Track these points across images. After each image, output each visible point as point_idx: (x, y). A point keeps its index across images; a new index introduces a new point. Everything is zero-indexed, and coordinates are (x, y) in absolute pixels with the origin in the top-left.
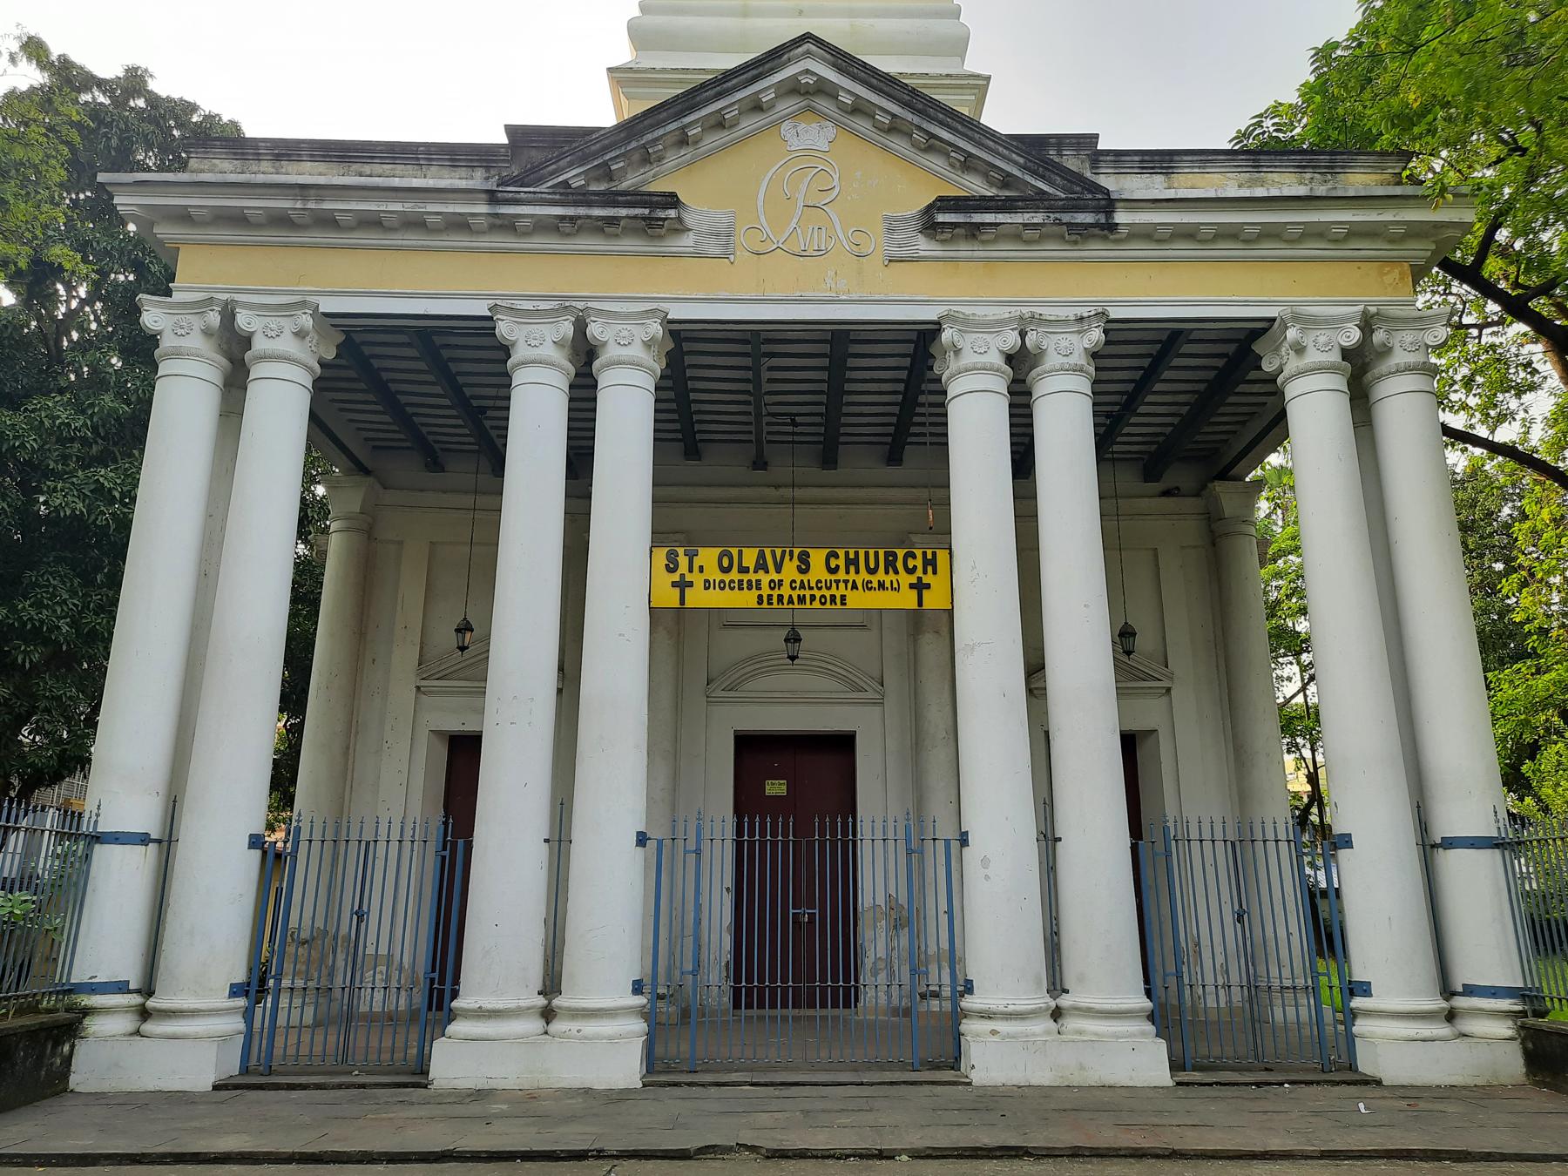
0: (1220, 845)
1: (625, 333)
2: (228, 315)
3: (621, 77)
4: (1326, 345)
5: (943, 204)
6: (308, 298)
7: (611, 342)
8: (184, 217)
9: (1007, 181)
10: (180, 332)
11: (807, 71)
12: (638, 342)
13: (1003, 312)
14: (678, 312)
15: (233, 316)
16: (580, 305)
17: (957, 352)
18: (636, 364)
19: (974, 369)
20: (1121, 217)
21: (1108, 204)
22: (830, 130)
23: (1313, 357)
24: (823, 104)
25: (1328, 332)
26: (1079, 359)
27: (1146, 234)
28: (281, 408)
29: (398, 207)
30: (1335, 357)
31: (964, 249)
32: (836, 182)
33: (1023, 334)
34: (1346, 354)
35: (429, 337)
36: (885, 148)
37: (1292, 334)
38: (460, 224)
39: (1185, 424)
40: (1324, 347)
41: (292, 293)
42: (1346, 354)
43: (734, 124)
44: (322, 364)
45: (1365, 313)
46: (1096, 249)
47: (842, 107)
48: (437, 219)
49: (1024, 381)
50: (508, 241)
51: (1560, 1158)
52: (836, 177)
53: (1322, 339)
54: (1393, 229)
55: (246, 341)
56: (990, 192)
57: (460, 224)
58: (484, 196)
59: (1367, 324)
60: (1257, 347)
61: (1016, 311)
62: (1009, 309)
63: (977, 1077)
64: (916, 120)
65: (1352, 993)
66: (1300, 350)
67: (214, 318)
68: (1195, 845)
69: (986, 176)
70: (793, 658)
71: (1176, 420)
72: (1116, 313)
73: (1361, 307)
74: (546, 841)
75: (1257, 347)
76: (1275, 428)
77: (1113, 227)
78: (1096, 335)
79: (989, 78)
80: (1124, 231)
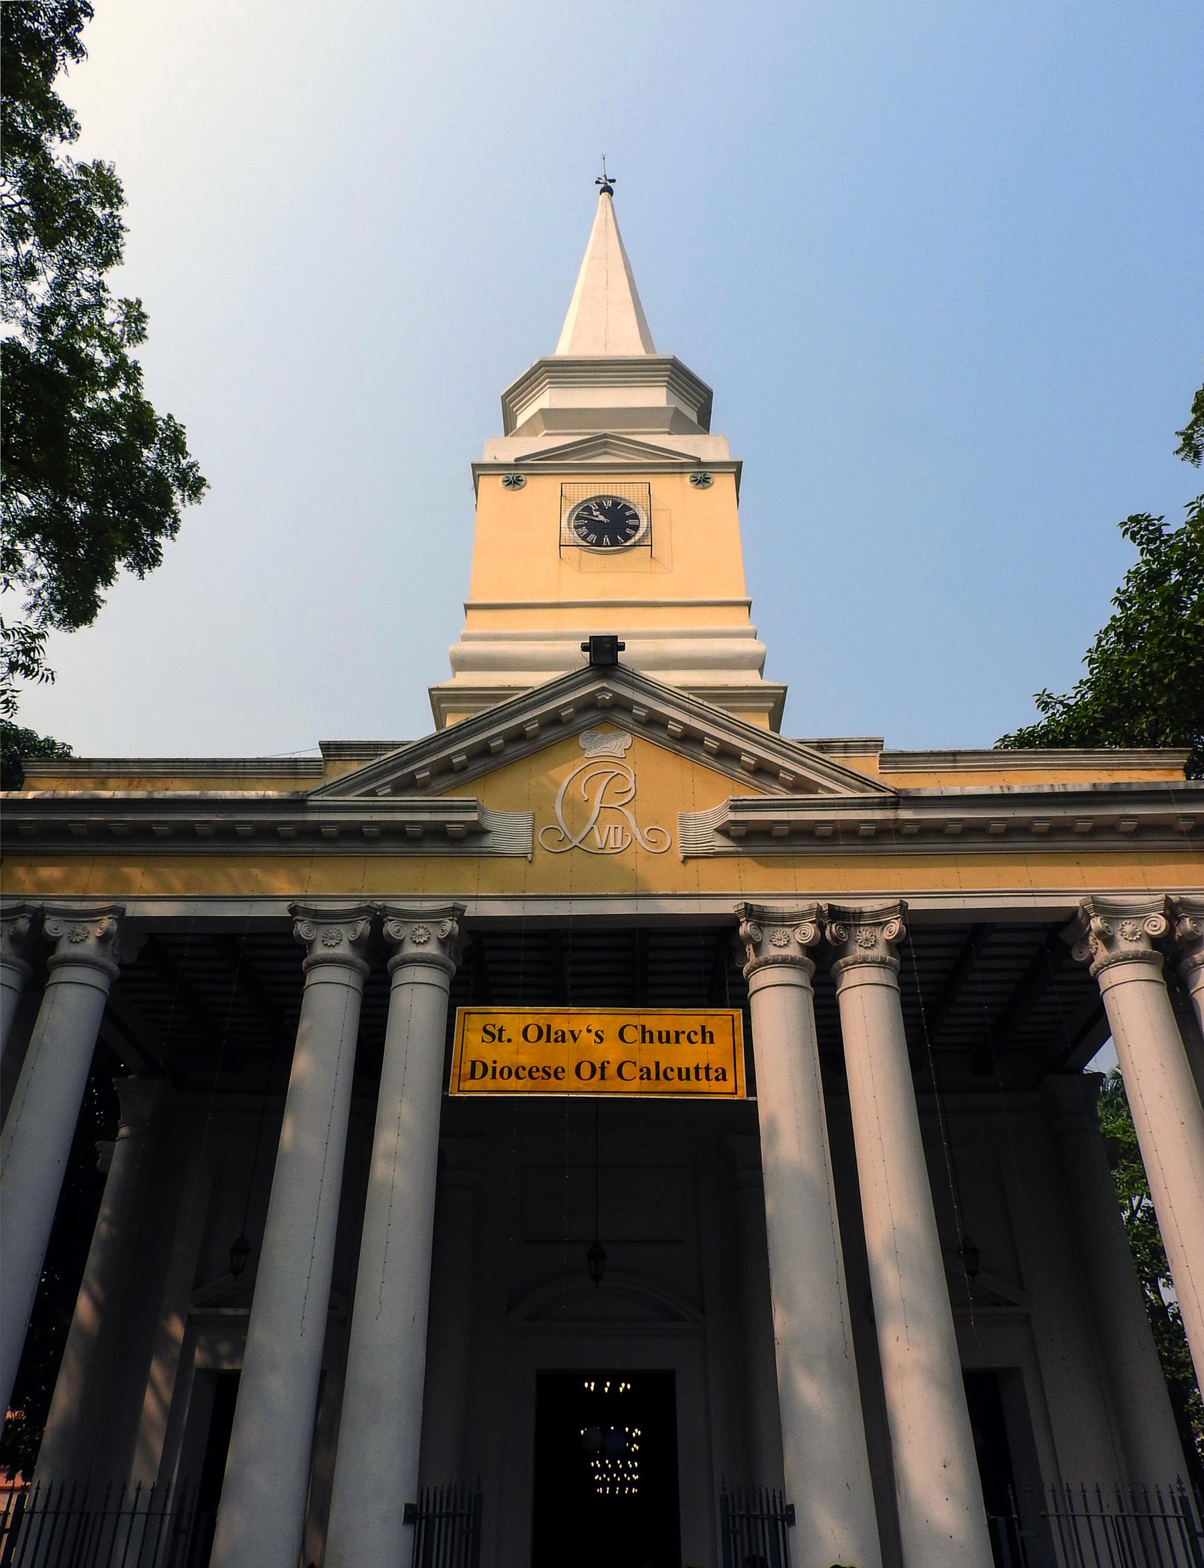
0: (1097, 1523)
1: (421, 931)
2: (38, 917)
3: (440, 699)
4: (1134, 934)
6: (27, 903)
7: (408, 939)
12: (345, 943)
13: (803, 905)
15: (42, 921)
16: (37, 904)
17: (758, 947)
19: (864, 961)
22: (627, 739)
23: (1125, 946)
24: (621, 717)
25: (1134, 922)
26: (880, 952)
29: (206, 817)
30: (1142, 947)
32: (632, 785)
33: (822, 928)
34: (1155, 942)
37: (1096, 923)
39: (1001, 1030)
43: (535, 737)
44: (121, 966)
45: (1167, 899)
47: (638, 721)
49: (828, 972)
50: (319, 848)
51: (108, 1566)
53: (1128, 929)
54: (822, 829)
55: (53, 944)
59: (1173, 911)
60: (1064, 936)
61: (813, 903)
62: (811, 902)
67: (23, 924)
68: (1082, 1522)
70: (597, 1278)
72: (914, 905)
73: (1162, 896)
75: (1064, 936)
76: (1094, 1026)
78: (895, 926)
79: (785, 688)
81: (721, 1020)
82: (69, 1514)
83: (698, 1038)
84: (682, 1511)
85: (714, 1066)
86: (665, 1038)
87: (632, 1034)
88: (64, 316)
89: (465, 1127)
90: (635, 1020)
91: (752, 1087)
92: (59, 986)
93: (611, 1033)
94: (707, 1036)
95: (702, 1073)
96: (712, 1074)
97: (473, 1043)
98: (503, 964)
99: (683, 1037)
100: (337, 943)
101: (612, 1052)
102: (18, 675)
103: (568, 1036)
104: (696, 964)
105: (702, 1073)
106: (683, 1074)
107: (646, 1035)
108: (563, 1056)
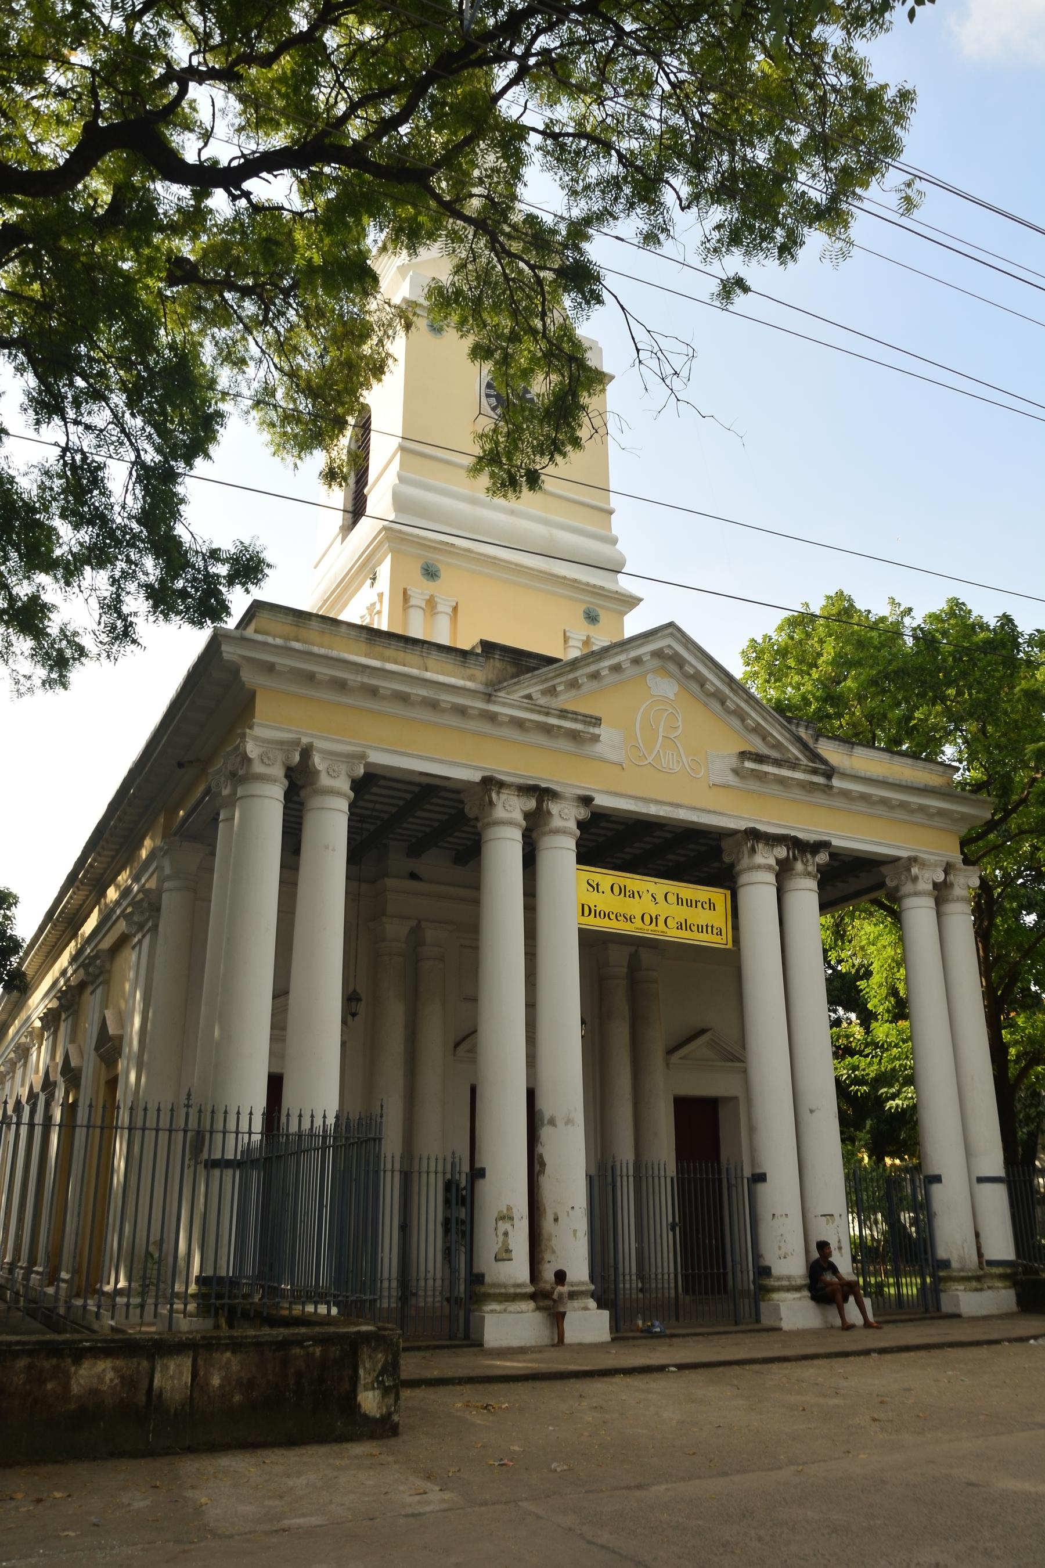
5: (743, 755)
8: (270, 668)
9: (777, 746)
10: (265, 760)
11: (669, 646)
14: (378, 758)
18: (345, 795)
20: (836, 782)
21: (830, 772)
27: (845, 794)
28: (332, 827)
31: (753, 785)
32: (680, 723)
35: (428, 791)
36: (706, 705)
38: (462, 711)
40: (927, 877)
41: (355, 744)
42: (935, 885)
46: (819, 798)
48: (476, 712)
50: (487, 728)
52: (680, 719)
56: (764, 750)
57: (462, 711)
58: (482, 696)
63: (786, 1325)
64: (732, 695)
65: (938, 1267)
66: (915, 879)
69: (764, 739)
71: (428, 830)
74: (938, 1179)
77: (831, 787)
80: (835, 790)
81: (718, 896)
82: (393, 1172)
83: (706, 906)
84: (89, 834)
85: (715, 926)
86: (690, 903)
87: (672, 899)
88: (253, 318)
89: (592, 944)
90: (676, 890)
91: (736, 941)
92: (757, 886)
93: (605, 886)
94: (712, 906)
95: (710, 929)
96: (715, 931)
97: (719, 918)
98: (617, 842)
99: (699, 904)
100: (510, 809)
101: (661, 909)
102: (28, 674)
103: (636, 894)
104: (696, 855)
105: (710, 929)
106: (700, 929)
107: (679, 901)
108: (634, 907)
